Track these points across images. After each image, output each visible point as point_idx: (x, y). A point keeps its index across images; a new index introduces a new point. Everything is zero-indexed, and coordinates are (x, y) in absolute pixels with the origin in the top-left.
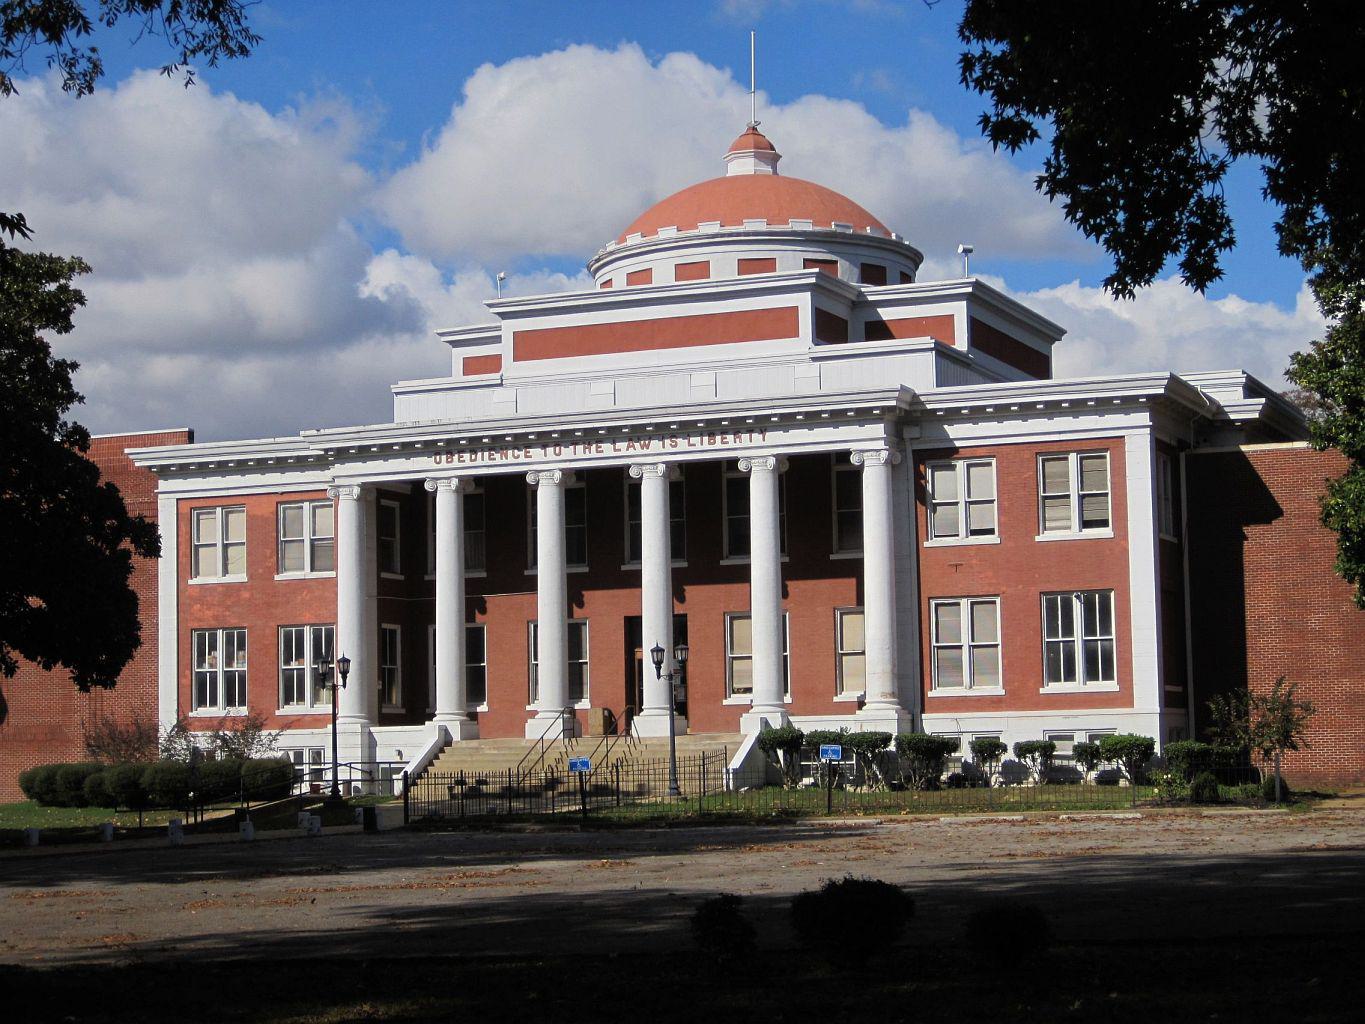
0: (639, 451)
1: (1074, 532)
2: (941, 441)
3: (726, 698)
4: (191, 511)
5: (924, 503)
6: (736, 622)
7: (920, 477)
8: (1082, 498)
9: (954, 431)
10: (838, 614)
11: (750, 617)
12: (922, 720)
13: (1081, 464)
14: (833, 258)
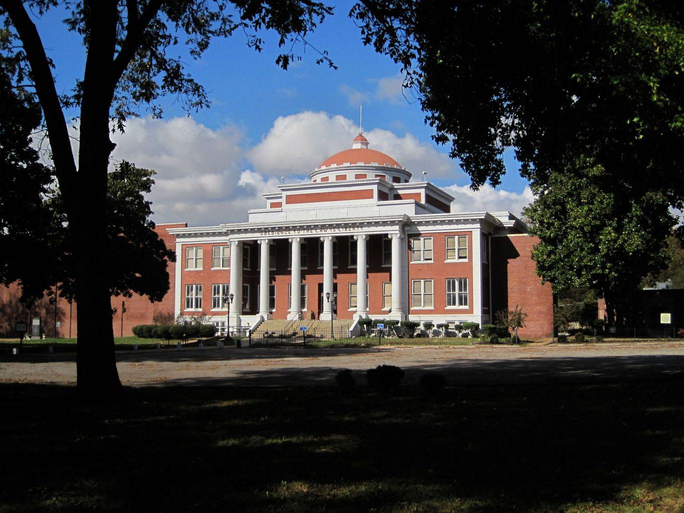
4: (185, 248)
5: (410, 250)
7: (409, 242)
8: (459, 249)
9: (421, 229)
11: (356, 284)
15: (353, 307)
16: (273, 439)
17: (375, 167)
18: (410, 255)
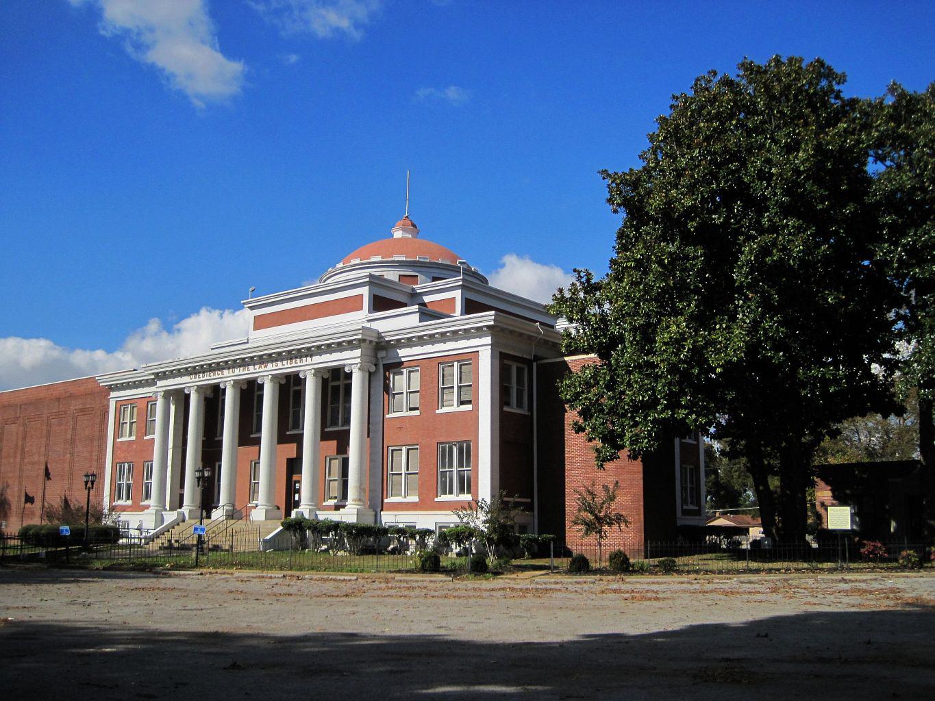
0: (264, 369)
1: (455, 408)
2: (395, 358)
3: (325, 501)
4: (121, 405)
5: (388, 394)
6: (332, 462)
7: (386, 378)
8: (460, 388)
9: (402, 352)
10: (328, 459)
12: (380, 515)
13: (461, 369)
14: (417, 274)
15: (331, 498)
16: (536, 690)
17: (398, 262)
18: (386, 403)
